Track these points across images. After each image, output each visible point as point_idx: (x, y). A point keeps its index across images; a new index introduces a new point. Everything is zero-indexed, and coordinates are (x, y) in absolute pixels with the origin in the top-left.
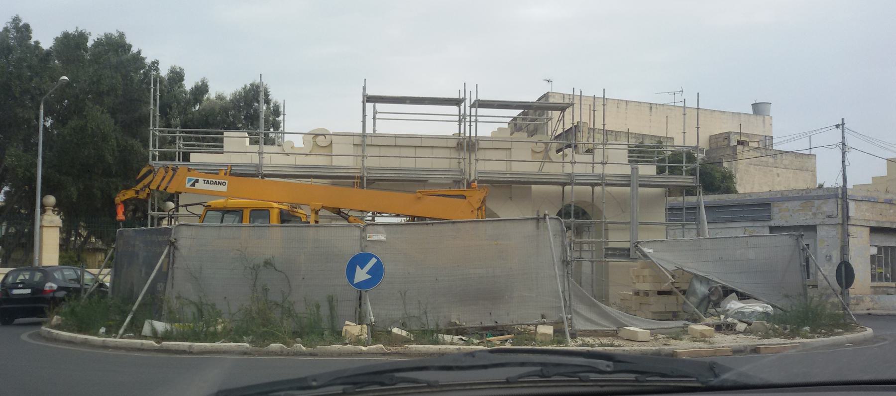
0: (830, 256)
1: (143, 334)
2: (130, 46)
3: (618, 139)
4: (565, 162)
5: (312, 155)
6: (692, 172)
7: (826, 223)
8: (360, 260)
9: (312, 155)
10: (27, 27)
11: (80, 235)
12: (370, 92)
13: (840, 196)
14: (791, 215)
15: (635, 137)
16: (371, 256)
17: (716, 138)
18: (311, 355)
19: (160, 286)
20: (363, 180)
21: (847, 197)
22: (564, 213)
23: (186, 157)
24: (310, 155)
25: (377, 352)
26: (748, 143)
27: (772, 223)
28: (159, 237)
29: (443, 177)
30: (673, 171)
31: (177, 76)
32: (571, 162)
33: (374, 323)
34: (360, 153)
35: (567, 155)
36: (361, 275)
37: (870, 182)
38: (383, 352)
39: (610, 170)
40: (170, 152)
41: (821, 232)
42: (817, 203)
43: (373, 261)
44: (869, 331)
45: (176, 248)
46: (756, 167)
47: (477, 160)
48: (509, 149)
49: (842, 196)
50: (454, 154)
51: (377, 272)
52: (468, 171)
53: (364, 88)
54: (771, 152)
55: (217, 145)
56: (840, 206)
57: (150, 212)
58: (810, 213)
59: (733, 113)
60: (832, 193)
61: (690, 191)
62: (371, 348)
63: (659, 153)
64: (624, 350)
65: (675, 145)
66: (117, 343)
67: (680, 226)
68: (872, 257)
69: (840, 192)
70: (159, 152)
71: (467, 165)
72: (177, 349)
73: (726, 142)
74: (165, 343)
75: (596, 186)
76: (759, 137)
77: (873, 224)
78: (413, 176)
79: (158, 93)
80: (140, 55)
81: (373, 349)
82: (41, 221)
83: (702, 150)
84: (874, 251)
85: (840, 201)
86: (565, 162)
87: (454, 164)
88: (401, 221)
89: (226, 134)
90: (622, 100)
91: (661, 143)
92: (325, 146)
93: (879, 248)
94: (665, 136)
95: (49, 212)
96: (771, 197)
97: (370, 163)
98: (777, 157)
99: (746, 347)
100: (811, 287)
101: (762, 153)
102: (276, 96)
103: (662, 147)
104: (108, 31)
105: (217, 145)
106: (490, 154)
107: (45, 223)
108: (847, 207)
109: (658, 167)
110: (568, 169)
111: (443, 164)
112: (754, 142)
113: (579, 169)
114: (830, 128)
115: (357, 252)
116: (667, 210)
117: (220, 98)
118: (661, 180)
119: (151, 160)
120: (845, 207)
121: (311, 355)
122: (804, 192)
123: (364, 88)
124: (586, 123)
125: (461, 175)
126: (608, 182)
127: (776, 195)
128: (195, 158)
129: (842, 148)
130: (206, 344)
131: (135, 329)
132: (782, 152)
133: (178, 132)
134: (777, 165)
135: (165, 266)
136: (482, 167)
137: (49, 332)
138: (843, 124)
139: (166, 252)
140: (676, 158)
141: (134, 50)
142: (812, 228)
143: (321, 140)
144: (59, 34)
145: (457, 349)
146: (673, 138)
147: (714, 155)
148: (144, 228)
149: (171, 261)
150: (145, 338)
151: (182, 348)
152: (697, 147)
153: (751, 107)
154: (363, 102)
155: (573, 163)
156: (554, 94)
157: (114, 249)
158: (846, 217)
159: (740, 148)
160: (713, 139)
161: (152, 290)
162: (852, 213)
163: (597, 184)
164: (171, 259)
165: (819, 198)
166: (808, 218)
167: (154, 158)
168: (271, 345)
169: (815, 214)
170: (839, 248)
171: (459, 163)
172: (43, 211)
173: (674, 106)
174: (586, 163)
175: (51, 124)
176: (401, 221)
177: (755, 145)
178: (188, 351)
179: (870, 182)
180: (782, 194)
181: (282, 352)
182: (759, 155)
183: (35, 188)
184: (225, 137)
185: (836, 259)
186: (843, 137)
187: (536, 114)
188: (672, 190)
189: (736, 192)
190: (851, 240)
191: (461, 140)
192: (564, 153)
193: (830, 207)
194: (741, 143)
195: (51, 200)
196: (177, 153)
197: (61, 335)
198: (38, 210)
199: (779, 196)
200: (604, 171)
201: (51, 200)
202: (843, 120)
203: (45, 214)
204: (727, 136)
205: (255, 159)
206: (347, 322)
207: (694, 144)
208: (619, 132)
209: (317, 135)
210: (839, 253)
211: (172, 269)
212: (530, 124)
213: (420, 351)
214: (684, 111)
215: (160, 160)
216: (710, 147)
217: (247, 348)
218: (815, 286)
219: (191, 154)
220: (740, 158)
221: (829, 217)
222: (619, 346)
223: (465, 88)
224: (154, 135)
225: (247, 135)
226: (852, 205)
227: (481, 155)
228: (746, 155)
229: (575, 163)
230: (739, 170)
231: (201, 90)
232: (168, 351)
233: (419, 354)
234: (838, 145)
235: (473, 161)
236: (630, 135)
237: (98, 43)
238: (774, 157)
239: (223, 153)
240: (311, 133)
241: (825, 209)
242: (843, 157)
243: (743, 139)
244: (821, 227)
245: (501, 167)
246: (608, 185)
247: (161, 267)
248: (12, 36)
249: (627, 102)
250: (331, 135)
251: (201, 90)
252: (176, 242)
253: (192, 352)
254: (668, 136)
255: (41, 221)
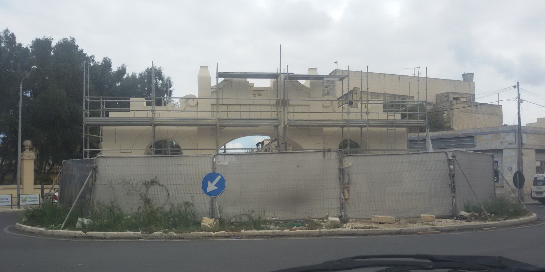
0: (511, 168)
1: (77, 226)
2: (78, 46)
3: (379, 98)
4: (344, 113)
5: (185, 111)
6: (423, 118)
7: (508, 148)
8: (211, 177)
9: (185, 111)
10: (13, 35)
11: (49, 164)
12: (221, 70)
13: (517, 131)
14: (487, 143)
15: (389, 97)
16: (217, 175)
17: (440, 96)
18: (180, 238)
19: (88, 196)
20: (217, 126)
21: (522, 131)
22: (343, 145)
23: (107, 115)
24: (184, 111)
25: (221, 235)
26: (460, 98)
27: (475, 149)
28: (86, 164)
29: (267, 123)
30: (411, 117)
31: (107, 64)
32: (347, 113)
33: (219, 218)
34: (215, 110)
35: (345, 108)
36: (211, 187)
37: (536, 121)
38: (225, 236)
39: (372, 117)
40: (98, 111)
41: (505, 153)
42: (502, 135)
43: (219, 178)
44: (534, 215)
45: (97, 172)
46: (465, 113)
47: (288, 112)
48: (308, 105)
49: (518, 130)
50: (274, 109)
51: (221, 185)
52: (282, 120)
53: (217, 68)
54: (474, 104)
55: (126, 106)
56: (517, 137)
57: (84, 149)
58: (499, 142)
59: (450, 80)
60: (512, 129)
61: (422, 129)
62: (217, 233)
63: (402, 106)
64: (378, 231)
65: (415, 100)
66: (60, 233)
67: (416, 151)
68: (537, 168)
69: (517, 128)
70: (90, 112)
71: (282, 116)
72: (96, 236)
73: (446, 98)
74: (89, 233)
75: (364, 127)
76: (466, 95)
77: (538, 148)
78: (248, 123)
79: (89, 75)
80: (83, 52)
81: (219, 234)
82: (22, 155)
83: (430, 104)
84: (538, 164)
85: (517, 134)
86: (344, 113)
87: (274, 115)
88: (248, 151)
89: (131, 99)
90: (381, 74)
91: (405, 99)
92: (193, 105)
93: (542, 162)
94: (408, 95)
95: (27, 150)
96: (474, 132)
97: (223, 115)
98: (478, 107)
99: (456, 228)
100: (500, 187)
101: (468, 105)
102: (166, 74)
103: (405, 102)
104: (65, 37)
105: (126, 106)
106: (297, 109)
107: (24, 157)
108: (521, 138)
109: (402, 115)
110: (346, 117)
111: (268, 116)
112: (464, 98)
113: (352, 117)
114: (510, 88)
115: (210, 171)
116: (408, 142)
117: (133, 76)
118: (405, 122)
119: (84, 116)
120: (520, 137)
121: (180, 238)
122: (495, 129)
123: (217, 68)
124: (359, 88)
125: (278, 122)
126: (370, 124)
127: (477, 131)
128: (113, 115)
129: (518, 101)
130: (114, 233)
131: (71, 225)
132: (481, 104)
133: (102, 99)
134: (478, 112)
135: (90, 183)
136: (291, 116)
137: (20, 226)
138: (518, 85)
139: (90, 174)
140: (413, 109)
141: (80, 48)
142: (500, 151)
143: (191, 102)
144: (34, 39)
145: (272, 232)
146: (413, 97)
147: (439, 107)
148: (78, 159)
149: (94, 180)
150: (78, 229)
151: (99, 236)
152: (426, 101)
153: (462, 76)
154: (217, 77)
155: (348, 113)
156: (339, 71)
157: (61, 172)
158: (521, 144)
159: (455, 102)
160: (438, 97)
161: (82, 197)
162: (524, 141)
163: (363, 126)
164: (94, 178)
165: (504, 132)
166: (498, 145)
167: (86, 116)
168: (154, 233)
169: (501, 142)
170: (516, 163)
171: (278, 114)
172: (23, 150)
173: (414, 76)
174: (357, 113)
175: (444, 113)
176: (248, 151)
177: (464, 100)
178: (103, 237)
179: (536, 121)
180: (481, 130)
181: (161, 237)
182: (467, 106)
183: (18, 136)
184: (131, 101)
185: (515, 170)
186: (519, 94)
187: (328, 83)
188: (411, 129)
189: (453, 129)
190: (524, 157)
191: (416, 105)
192: (343, 107)
193: (511, 138)
194: (456, 99)
195: (28, 143)
196: (101, 112)
197: (27, 228)
198: (20, 149)
199: (479, 131)
200: (368, 117)
201: (28, 143)
202: (518, 83)
203: (25, 151)
204: (447, 95)
205: (150, 115)
206: (203, 218)
207: (424, 99)
208: (379, 93)
209: (189, 99)
210: (517, 165)
211: (95, 185)
212: (325, 89)
213: (248, 234)
214: (418, 79)
215: (90, 116)
216: (437, 102)
217: (140, 235)
218: (502, 187)
219: (110, 112)
220: (455, 108)
221: (511, 144)
222: (377, 228)
223: (288, 68)
224: (86, 101)
225: (145, 100)
226: (524, 136)
227: (291, 109)
228: (459, 106)
229: (350, 113)
230: (454, 115)
231: (122, 71)
232: (90, 237)
233: (248, 236)
234: (515, 99)
235: (286, 113)
236: (386, 95)
237: (59, 45)
238: (476, 107)
239: (129, 111)
240: (184, 97)
241: (508, 139)
242: (519, 106)
243: (457, 96)
244: (505, 150)
245: (303, 117)
246: (370, 126)
247: (88, 183)
248: (4, 41)
249: (384, 74)
250: (197, 98)
251: (122, 71)
252: (97, 167)
253: (105, 238)
254: (410, 95)
255: (22, 155)
